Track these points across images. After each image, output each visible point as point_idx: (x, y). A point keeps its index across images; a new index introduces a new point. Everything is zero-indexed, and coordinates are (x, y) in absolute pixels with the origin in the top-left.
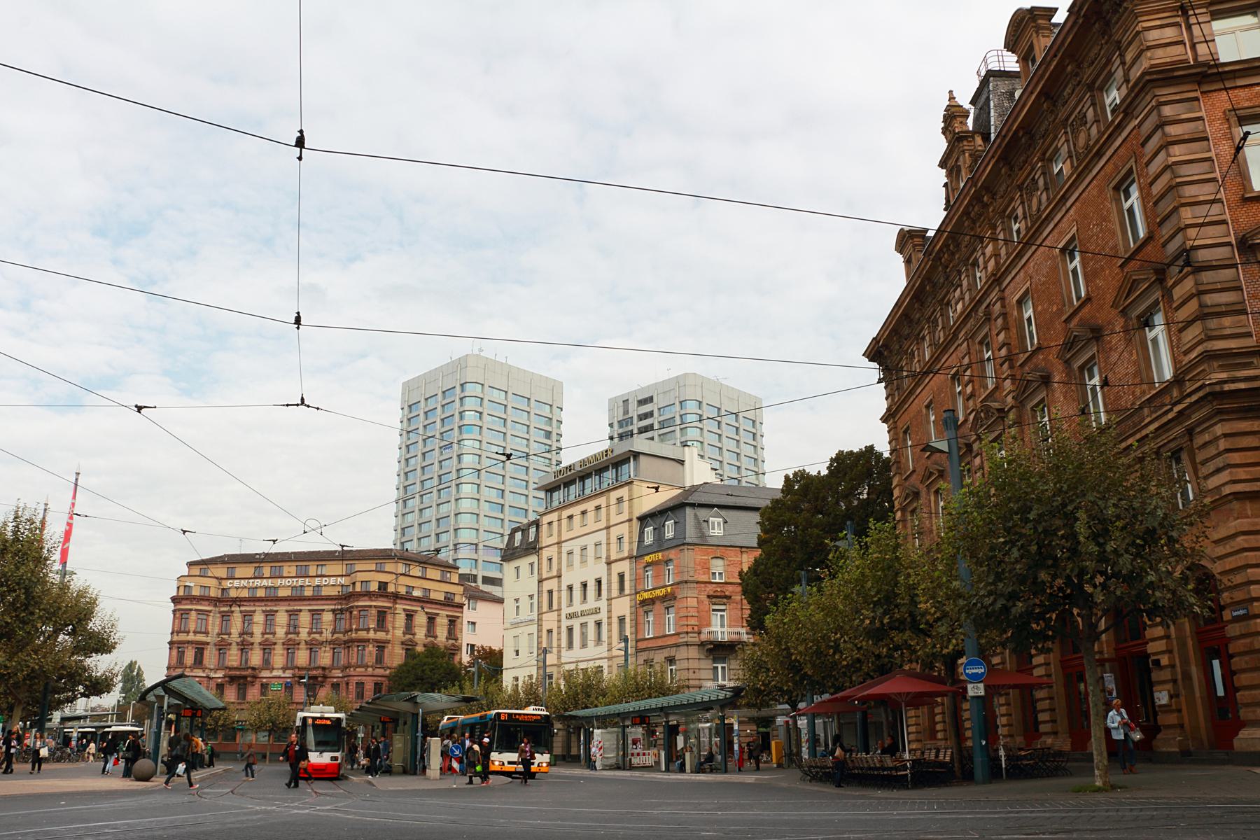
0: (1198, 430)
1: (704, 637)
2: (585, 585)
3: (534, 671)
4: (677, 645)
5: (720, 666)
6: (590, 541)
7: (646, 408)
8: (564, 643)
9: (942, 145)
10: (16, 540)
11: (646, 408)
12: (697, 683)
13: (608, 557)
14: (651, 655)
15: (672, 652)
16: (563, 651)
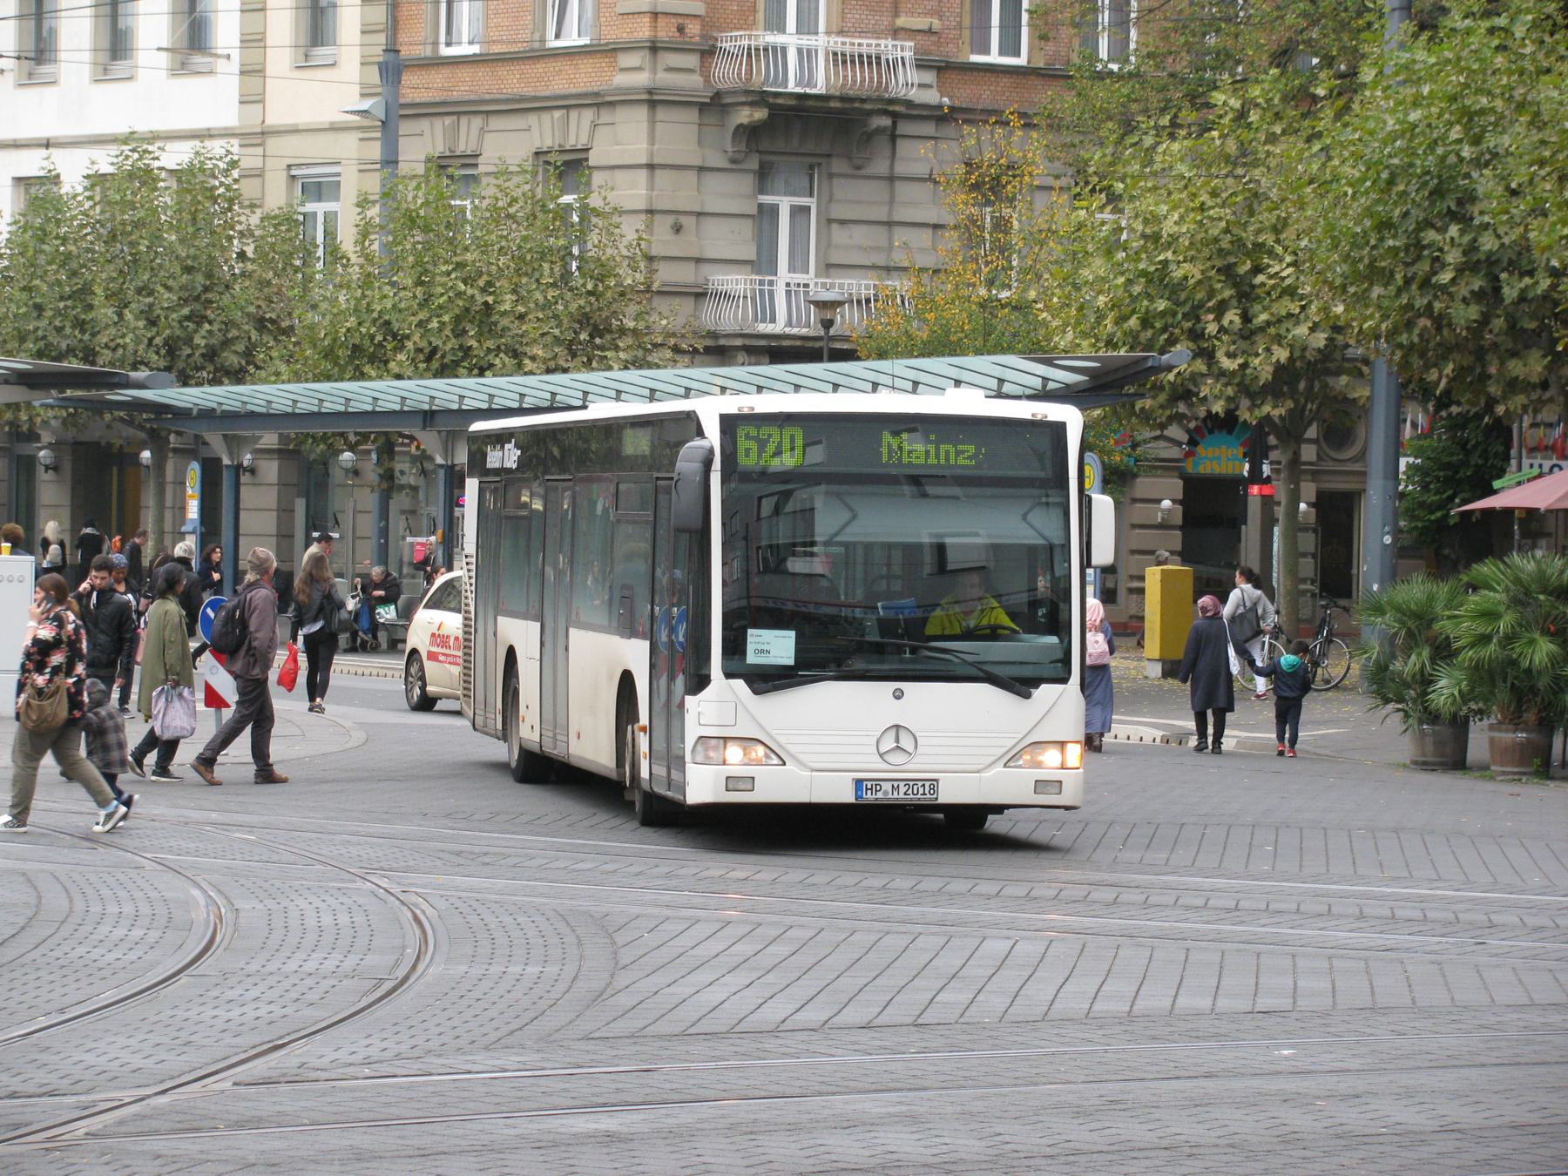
0: (300, 505)
1: (726, 74)
4: (600, 102)
5: (785, 204)
7: (368, 1041)
9: (142, 127)
11: (368, 1041)
12: (683, 275)
14: (468, 135)
15: (578, 129)
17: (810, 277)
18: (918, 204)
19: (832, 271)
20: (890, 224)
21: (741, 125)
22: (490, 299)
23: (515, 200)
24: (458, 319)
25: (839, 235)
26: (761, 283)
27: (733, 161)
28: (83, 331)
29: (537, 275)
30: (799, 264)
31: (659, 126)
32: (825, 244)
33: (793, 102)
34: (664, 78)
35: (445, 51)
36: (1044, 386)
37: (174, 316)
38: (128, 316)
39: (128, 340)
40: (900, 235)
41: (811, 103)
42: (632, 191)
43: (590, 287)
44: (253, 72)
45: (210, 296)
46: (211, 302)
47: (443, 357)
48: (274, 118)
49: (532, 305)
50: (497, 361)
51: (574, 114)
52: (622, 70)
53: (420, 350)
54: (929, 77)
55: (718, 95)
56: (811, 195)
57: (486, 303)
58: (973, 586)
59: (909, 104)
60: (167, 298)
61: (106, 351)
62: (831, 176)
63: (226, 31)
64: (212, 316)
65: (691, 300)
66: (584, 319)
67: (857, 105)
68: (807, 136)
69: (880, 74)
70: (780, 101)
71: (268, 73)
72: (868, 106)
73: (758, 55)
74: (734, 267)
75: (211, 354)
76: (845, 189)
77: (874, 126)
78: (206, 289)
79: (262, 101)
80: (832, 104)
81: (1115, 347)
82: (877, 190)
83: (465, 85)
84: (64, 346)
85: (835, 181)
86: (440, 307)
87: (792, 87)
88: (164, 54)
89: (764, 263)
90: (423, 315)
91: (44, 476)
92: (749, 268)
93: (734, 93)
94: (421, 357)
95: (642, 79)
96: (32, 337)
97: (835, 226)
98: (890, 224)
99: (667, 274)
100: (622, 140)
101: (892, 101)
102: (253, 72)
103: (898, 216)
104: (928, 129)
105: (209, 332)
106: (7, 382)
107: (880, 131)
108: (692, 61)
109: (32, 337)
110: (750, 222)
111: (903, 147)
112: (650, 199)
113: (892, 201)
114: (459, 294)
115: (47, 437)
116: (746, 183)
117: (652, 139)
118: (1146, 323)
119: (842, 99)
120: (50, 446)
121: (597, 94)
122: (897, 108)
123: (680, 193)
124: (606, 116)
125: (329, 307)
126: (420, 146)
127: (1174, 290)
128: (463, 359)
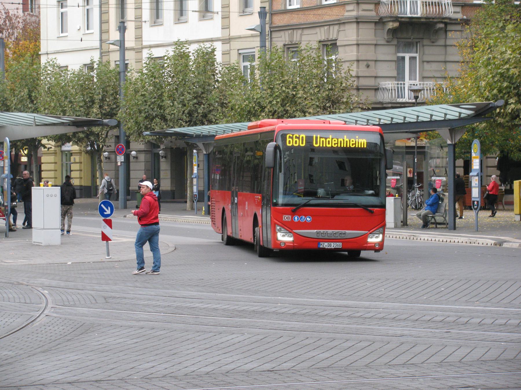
1: (384, 11)
3: (96, 56)
4: (341, 23)
5: (407, 56)
8: (146, 14)
9: (183, 39)
10: (262, 207)
12: (370, 82)
14: (297, 36)
15: (333, 33)
16: (146, 27)
17: (417, 82)
18: (454, 55)
19: (425, 79)
20: (445, 62)
21: (389, 29)
22: (294, 93)
23: (304, 58)
24: (283, 100)
25: (427, 66)
26: (398, 84)
27: (388, 42)
28: (161, 109)
29: (311, 84)
30: (413, 77)
31: (360, 30)
32: (422, 70)
33: (408, 20)
34: (361, 13)
35: (289, 8)
36: (460, 115)
37: (191, 103)
38: (175, 103)
39: (175, 112)
40: (450, 66)
41: (414, 20)
42: (351, 54)
43: (330, 87)
44: (226, 17)
45: (203, 95)
46: (204, 98)
47: (278, 113)
48: (233, 34)
49: (309, 95)
50: (297, 114)
51: (331, 27)
52: (347, 11)
53: (271, 112)
54: (458, 9)
55: (381, 18)
56: (417, 53)
57: (293, 94)
58: (236, 188)
59: (450, 19)
60: (188, 97)
61: (168, 116)
62: (423, 46)
63: (216, 4)
64: (204, 102)
65: (373, 91)
66: (328, 98)
67: (431, 20)
68: (413, 32)
69: (442, 9)
70: (403, 20)
71: (110, 3)
72: (435, 20)
73: (394, 4)
74: (387, 79)
75: (205, 116)
76: (429, 50)
77: (438, 27)
78: (202, 93)
79: (229, 28)
80: (422, 20)
81: (489, 100)
82: (441, 50)
83: (295, 19)
84: (154, 114)
85: (425, 47)
86: (277, 96)
87: (409, 15)
88: (197, 13)
89: (400, 76)
90: (271, 99)
91: (162, 160)
92: (394, 79)
93: (386, 17)
94: (270, 114)
95: (354, 13)
96: (143, 112)
97: (425, 63)
98: (445, 62)
99: (364, 82)
100: (348, 35)
101: (446, 18)
102: (226, 17)
103: (447, 60)
104: (459, 28)
105: (204, 108)
106: (69, 125)
107: (440, 29)
108: (372, 7)
109: (143, 112)
110: (394, 63)
111: (450, 35)
112: (358, 56)
113: (446, 54)
114: (284, 91)
115: (162, 147)
116: (392, 49)
117: (358, 35)
118: (500, 91)
119: (426, 18)
120: (163, 149)
121: (339, 20)
122: (446, 21)
123: (369, 53)
124: (342, 28)
125: (238, 98)
126: (281, 40)
127: (510, 79)
128: (285, 114)
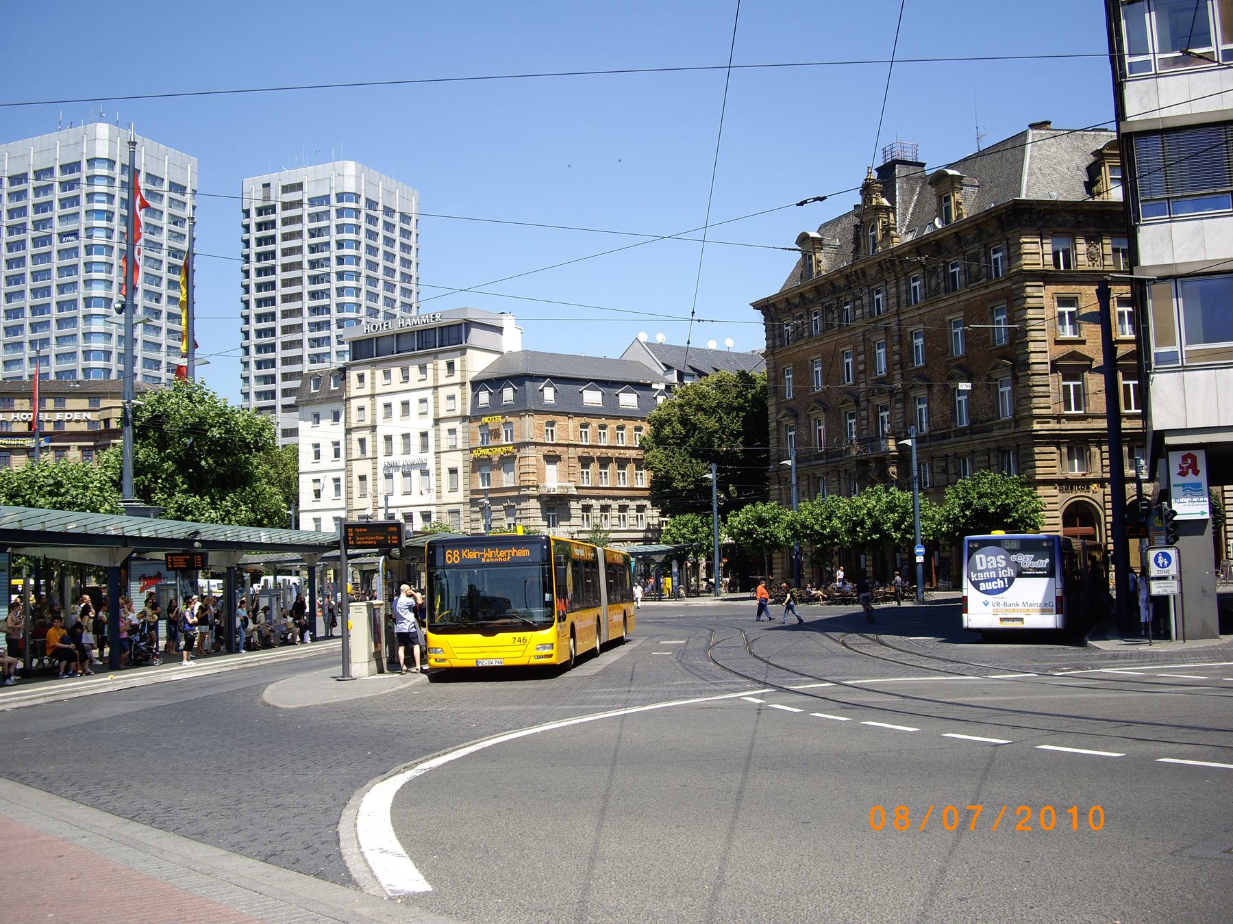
2: (406, 436)
6: (414, 398)
13: (436, 413)
